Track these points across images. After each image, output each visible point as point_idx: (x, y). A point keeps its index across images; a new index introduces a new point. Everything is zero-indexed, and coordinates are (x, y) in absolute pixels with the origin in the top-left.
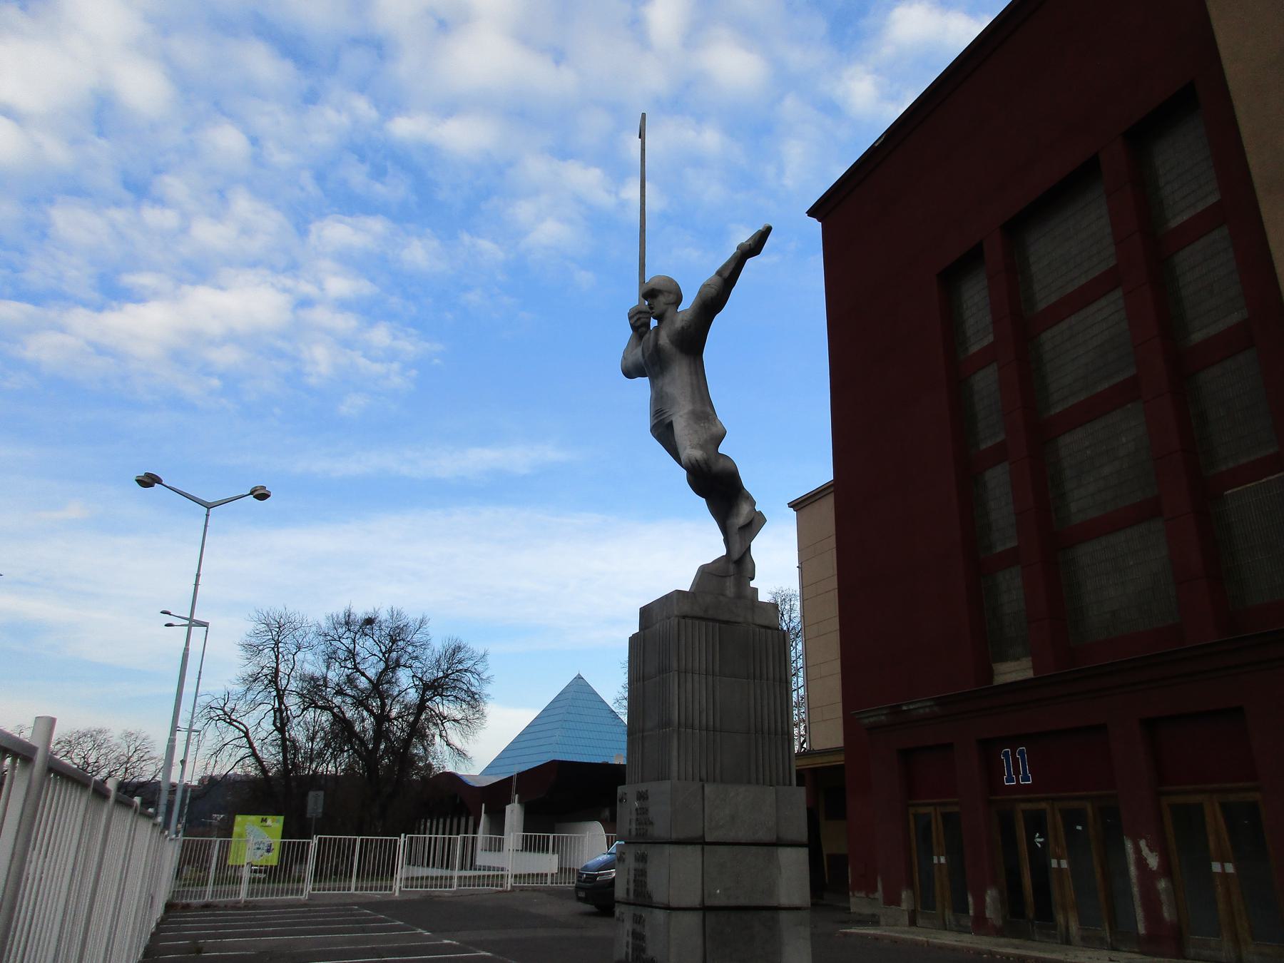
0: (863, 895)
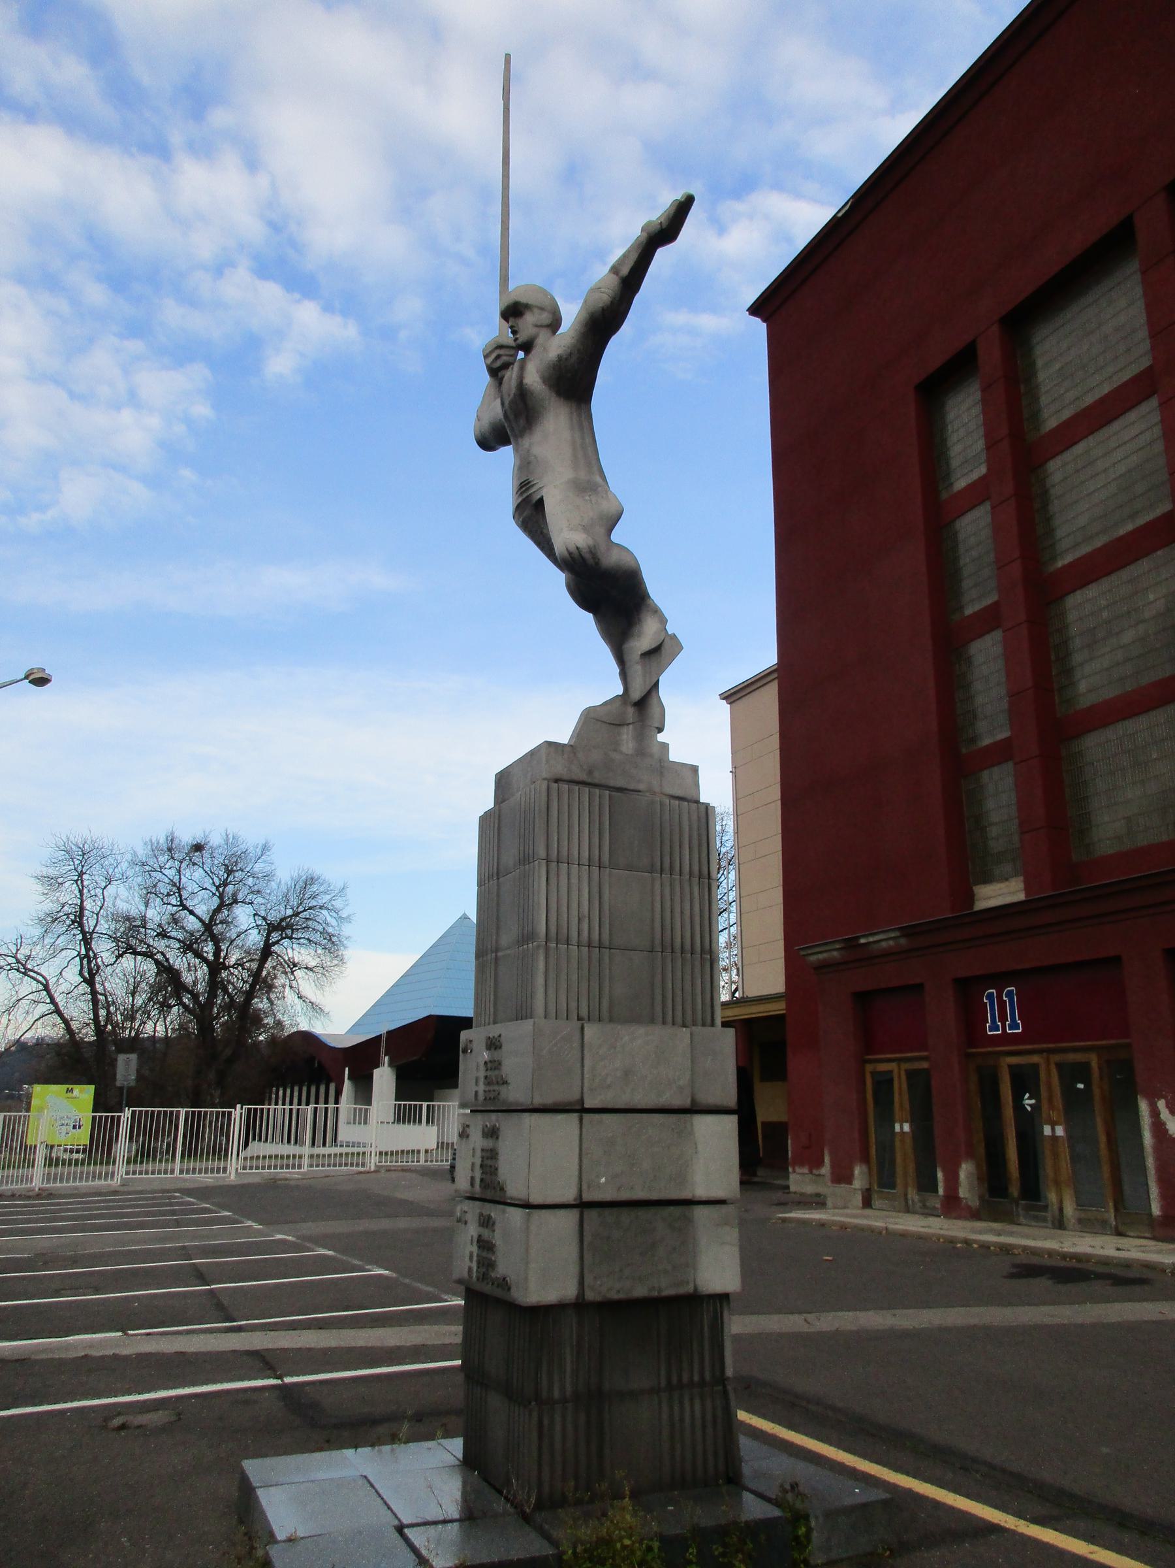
0: (806, 1170)
